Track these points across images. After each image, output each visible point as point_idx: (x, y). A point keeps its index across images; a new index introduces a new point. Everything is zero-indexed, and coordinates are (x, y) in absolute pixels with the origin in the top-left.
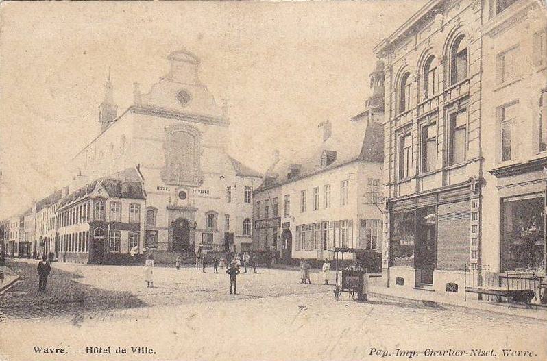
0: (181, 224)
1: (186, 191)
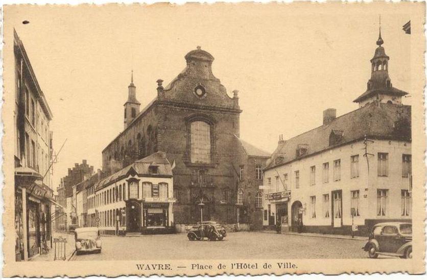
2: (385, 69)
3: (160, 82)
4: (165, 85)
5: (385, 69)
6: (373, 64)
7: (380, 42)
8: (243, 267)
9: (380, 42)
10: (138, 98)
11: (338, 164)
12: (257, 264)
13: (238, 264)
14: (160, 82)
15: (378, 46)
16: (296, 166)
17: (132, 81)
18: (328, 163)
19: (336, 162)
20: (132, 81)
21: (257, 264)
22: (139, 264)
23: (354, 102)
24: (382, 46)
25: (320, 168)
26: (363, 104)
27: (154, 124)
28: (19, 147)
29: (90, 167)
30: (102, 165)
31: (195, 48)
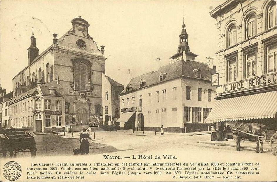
0: (83, 112)
1: (85, 94)
2: (186, 41)
3: (55, 35)
4: (58, 38)
5: (186, 41)
6: (181, 38)
7: (184, 26)
8: (143, 158)
9: (184, 26)
10: (38, 46)
11: (150, 95)
12: (152, 156)
13: (139, 155)
14: (55, 35)
15: (183, 28)
16: (139, 93)
17: (33, 34)
18: (151, 93)
19: (150, 94)
20: (33, 34)
21: (152, 156)
22: (105, 155)
23: (198, 56)
24: (185, 28)
25: (154, 94)
26: (176, 60)
27: (52, 63)
28: (265, 40)
29: (3, 89)
30: (12, 87)
31: (78, 17)
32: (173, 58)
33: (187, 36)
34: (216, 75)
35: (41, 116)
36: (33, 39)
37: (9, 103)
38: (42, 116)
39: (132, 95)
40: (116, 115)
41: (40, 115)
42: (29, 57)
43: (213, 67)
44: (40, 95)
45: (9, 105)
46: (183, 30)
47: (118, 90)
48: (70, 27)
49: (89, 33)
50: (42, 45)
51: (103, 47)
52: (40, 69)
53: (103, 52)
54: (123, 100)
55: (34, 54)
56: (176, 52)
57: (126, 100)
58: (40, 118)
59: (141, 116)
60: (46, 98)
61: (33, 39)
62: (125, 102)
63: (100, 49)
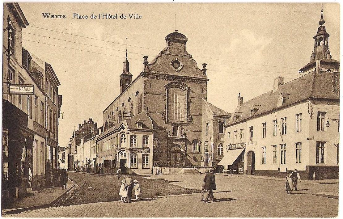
3: (146, 58)
10: (131, 71)
14: (146, 58)
16: (249, 123)
26: (307, 73)
32: (302, 70)
33: (327, 36)
34: (329, 97)
35: (126, 154)
36: (127, 64)
37: (97, 140)
38: (127, 155)
39: (240, 126)
40: (219, 154)
41: (125, 154)
42: (121, 86)
43: (90, 119)
44: (126, 130)
45: (97, 142)
46: (319, 30)
47: (221, 122)
48: (163, 45)
49: (186, 49)
50: (136, 69)
51: (204, 65)
52: (130, 99)
53: (205, 71)
54: (230, 133)
55: (126, 80)
56: (308, 61)
57: (232, 133)
58: (125, 156)
59: (252, 154)
60: (131, 133)
61: (127, 64)
62: (231, 135)
63: (201, 67)
